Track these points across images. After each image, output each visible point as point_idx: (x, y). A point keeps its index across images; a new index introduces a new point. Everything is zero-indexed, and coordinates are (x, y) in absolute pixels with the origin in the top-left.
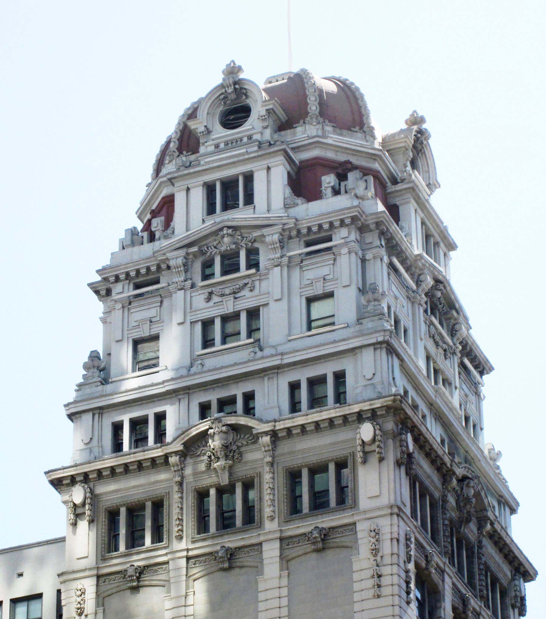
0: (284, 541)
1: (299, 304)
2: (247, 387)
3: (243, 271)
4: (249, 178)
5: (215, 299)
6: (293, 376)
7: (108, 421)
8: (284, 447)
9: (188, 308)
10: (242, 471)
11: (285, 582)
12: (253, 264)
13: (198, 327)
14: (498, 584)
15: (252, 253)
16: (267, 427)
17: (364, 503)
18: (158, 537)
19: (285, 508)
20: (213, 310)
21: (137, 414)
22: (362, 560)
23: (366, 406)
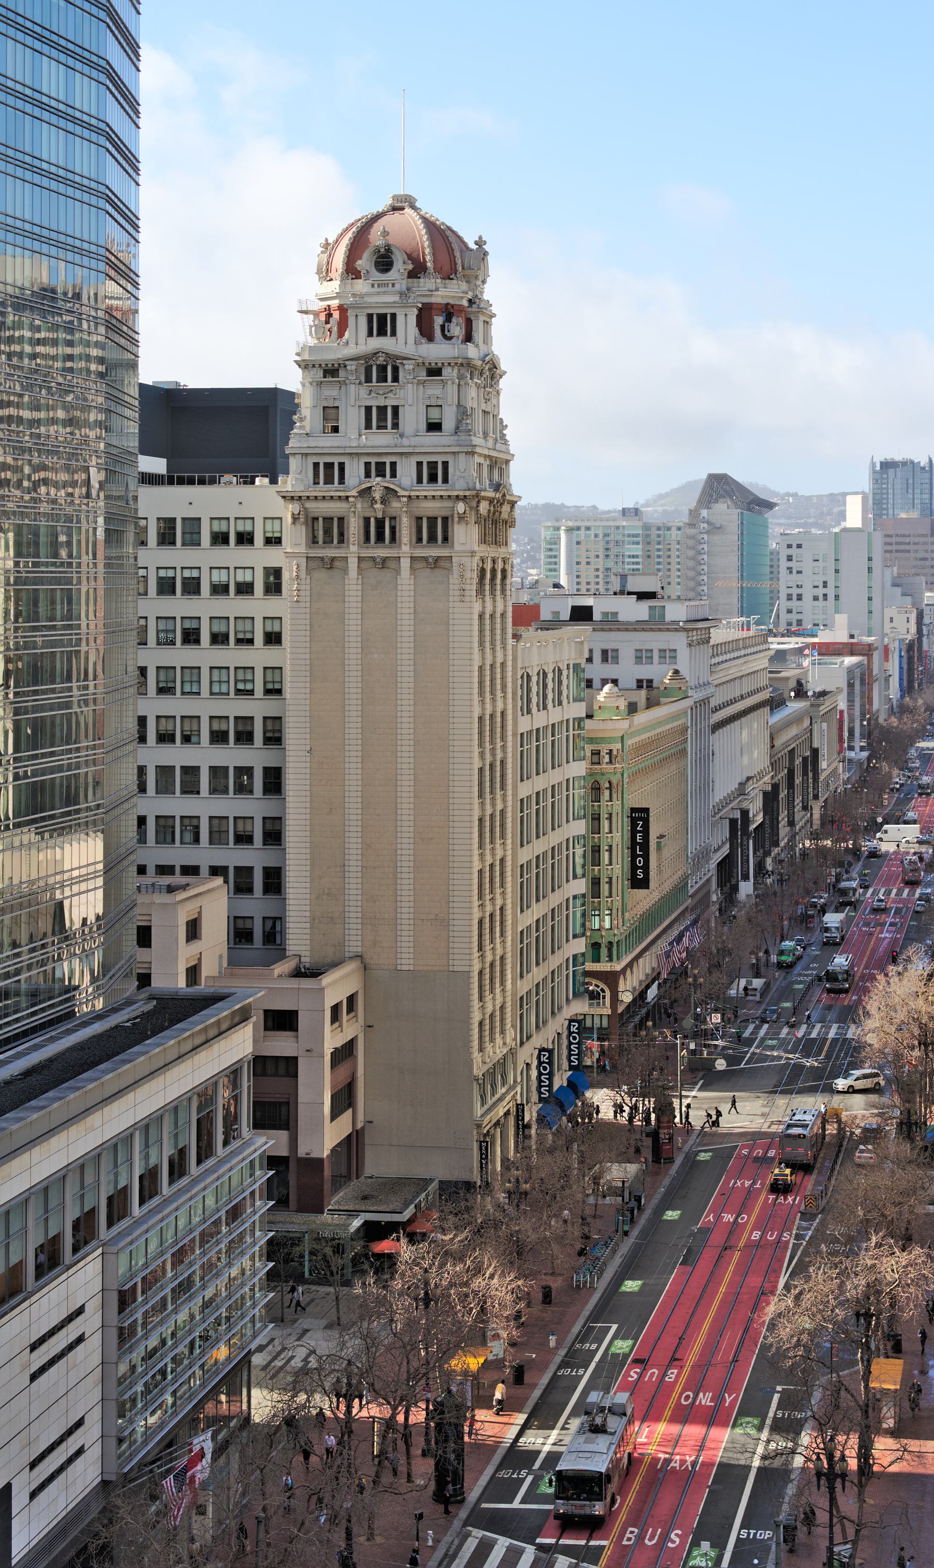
0: (413, 558)
1: (422, 409)
2: (373, 290)
3: (389, 383)
4: (394, 316)
5: (373, 395)
6: (420, 459)
7: (311, 461)
8: (415, 504)
9: (358, 398)
10: (391, 512)
11: (412, 582)
12: (396, 379)
13: (363, 410)
14: (484, 1505)
15: (396, 370)
16: (406, 493)
17: (457, 547)
18: (341, 541)
19: (414, 539)
20: (374, 403)
21: (329, 460)
22: (454, 579)
23: (461, 493)
